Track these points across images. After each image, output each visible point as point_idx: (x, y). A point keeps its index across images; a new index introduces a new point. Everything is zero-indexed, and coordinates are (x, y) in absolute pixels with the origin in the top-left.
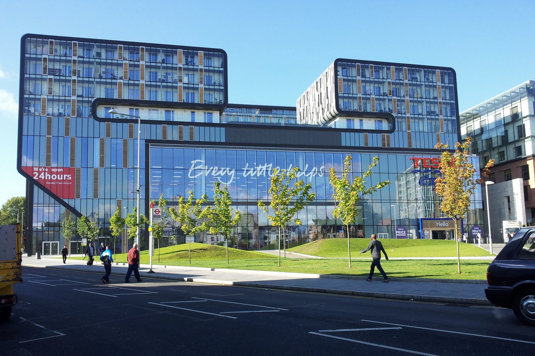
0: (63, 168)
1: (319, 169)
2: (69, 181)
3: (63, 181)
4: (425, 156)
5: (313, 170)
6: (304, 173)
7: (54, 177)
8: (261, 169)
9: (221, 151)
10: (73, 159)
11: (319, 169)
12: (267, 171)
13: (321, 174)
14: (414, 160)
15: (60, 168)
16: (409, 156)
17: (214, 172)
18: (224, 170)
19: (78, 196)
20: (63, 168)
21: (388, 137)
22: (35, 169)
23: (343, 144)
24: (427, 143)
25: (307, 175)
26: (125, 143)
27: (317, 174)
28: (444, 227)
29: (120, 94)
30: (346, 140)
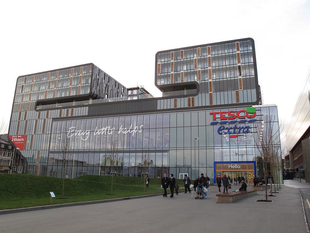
0: (222, 134)
1: (139, 127)
2: (23, 142)
3: (21, 142)
4: (223, 111)
5: (136, 128)
6: (129, 130)
7: (18, 140)
8: (104, 130)
9: (88, 121)
10: (25, 132)
11: (139, 127)
12: (107, 131)
13: (140, 131)
14: (213, 114)
15: (21, 135)
16: (208, 112)
17: (79, 133)
18: (100, 131)
19: (25, 149)
20: (222, 134)
21: (193, 99)
22: (13, 137)
23: (158, 108)
24: (200, 101)
25: (131, 132)
26: (45, 120)
27: (138, 131)
28: (236, 169)
29: (182, 80)
30: (160, 105)
